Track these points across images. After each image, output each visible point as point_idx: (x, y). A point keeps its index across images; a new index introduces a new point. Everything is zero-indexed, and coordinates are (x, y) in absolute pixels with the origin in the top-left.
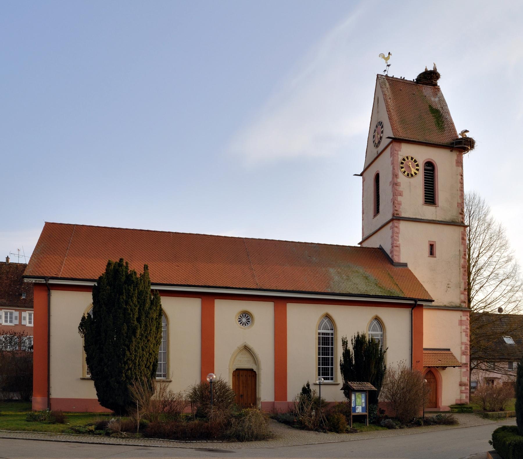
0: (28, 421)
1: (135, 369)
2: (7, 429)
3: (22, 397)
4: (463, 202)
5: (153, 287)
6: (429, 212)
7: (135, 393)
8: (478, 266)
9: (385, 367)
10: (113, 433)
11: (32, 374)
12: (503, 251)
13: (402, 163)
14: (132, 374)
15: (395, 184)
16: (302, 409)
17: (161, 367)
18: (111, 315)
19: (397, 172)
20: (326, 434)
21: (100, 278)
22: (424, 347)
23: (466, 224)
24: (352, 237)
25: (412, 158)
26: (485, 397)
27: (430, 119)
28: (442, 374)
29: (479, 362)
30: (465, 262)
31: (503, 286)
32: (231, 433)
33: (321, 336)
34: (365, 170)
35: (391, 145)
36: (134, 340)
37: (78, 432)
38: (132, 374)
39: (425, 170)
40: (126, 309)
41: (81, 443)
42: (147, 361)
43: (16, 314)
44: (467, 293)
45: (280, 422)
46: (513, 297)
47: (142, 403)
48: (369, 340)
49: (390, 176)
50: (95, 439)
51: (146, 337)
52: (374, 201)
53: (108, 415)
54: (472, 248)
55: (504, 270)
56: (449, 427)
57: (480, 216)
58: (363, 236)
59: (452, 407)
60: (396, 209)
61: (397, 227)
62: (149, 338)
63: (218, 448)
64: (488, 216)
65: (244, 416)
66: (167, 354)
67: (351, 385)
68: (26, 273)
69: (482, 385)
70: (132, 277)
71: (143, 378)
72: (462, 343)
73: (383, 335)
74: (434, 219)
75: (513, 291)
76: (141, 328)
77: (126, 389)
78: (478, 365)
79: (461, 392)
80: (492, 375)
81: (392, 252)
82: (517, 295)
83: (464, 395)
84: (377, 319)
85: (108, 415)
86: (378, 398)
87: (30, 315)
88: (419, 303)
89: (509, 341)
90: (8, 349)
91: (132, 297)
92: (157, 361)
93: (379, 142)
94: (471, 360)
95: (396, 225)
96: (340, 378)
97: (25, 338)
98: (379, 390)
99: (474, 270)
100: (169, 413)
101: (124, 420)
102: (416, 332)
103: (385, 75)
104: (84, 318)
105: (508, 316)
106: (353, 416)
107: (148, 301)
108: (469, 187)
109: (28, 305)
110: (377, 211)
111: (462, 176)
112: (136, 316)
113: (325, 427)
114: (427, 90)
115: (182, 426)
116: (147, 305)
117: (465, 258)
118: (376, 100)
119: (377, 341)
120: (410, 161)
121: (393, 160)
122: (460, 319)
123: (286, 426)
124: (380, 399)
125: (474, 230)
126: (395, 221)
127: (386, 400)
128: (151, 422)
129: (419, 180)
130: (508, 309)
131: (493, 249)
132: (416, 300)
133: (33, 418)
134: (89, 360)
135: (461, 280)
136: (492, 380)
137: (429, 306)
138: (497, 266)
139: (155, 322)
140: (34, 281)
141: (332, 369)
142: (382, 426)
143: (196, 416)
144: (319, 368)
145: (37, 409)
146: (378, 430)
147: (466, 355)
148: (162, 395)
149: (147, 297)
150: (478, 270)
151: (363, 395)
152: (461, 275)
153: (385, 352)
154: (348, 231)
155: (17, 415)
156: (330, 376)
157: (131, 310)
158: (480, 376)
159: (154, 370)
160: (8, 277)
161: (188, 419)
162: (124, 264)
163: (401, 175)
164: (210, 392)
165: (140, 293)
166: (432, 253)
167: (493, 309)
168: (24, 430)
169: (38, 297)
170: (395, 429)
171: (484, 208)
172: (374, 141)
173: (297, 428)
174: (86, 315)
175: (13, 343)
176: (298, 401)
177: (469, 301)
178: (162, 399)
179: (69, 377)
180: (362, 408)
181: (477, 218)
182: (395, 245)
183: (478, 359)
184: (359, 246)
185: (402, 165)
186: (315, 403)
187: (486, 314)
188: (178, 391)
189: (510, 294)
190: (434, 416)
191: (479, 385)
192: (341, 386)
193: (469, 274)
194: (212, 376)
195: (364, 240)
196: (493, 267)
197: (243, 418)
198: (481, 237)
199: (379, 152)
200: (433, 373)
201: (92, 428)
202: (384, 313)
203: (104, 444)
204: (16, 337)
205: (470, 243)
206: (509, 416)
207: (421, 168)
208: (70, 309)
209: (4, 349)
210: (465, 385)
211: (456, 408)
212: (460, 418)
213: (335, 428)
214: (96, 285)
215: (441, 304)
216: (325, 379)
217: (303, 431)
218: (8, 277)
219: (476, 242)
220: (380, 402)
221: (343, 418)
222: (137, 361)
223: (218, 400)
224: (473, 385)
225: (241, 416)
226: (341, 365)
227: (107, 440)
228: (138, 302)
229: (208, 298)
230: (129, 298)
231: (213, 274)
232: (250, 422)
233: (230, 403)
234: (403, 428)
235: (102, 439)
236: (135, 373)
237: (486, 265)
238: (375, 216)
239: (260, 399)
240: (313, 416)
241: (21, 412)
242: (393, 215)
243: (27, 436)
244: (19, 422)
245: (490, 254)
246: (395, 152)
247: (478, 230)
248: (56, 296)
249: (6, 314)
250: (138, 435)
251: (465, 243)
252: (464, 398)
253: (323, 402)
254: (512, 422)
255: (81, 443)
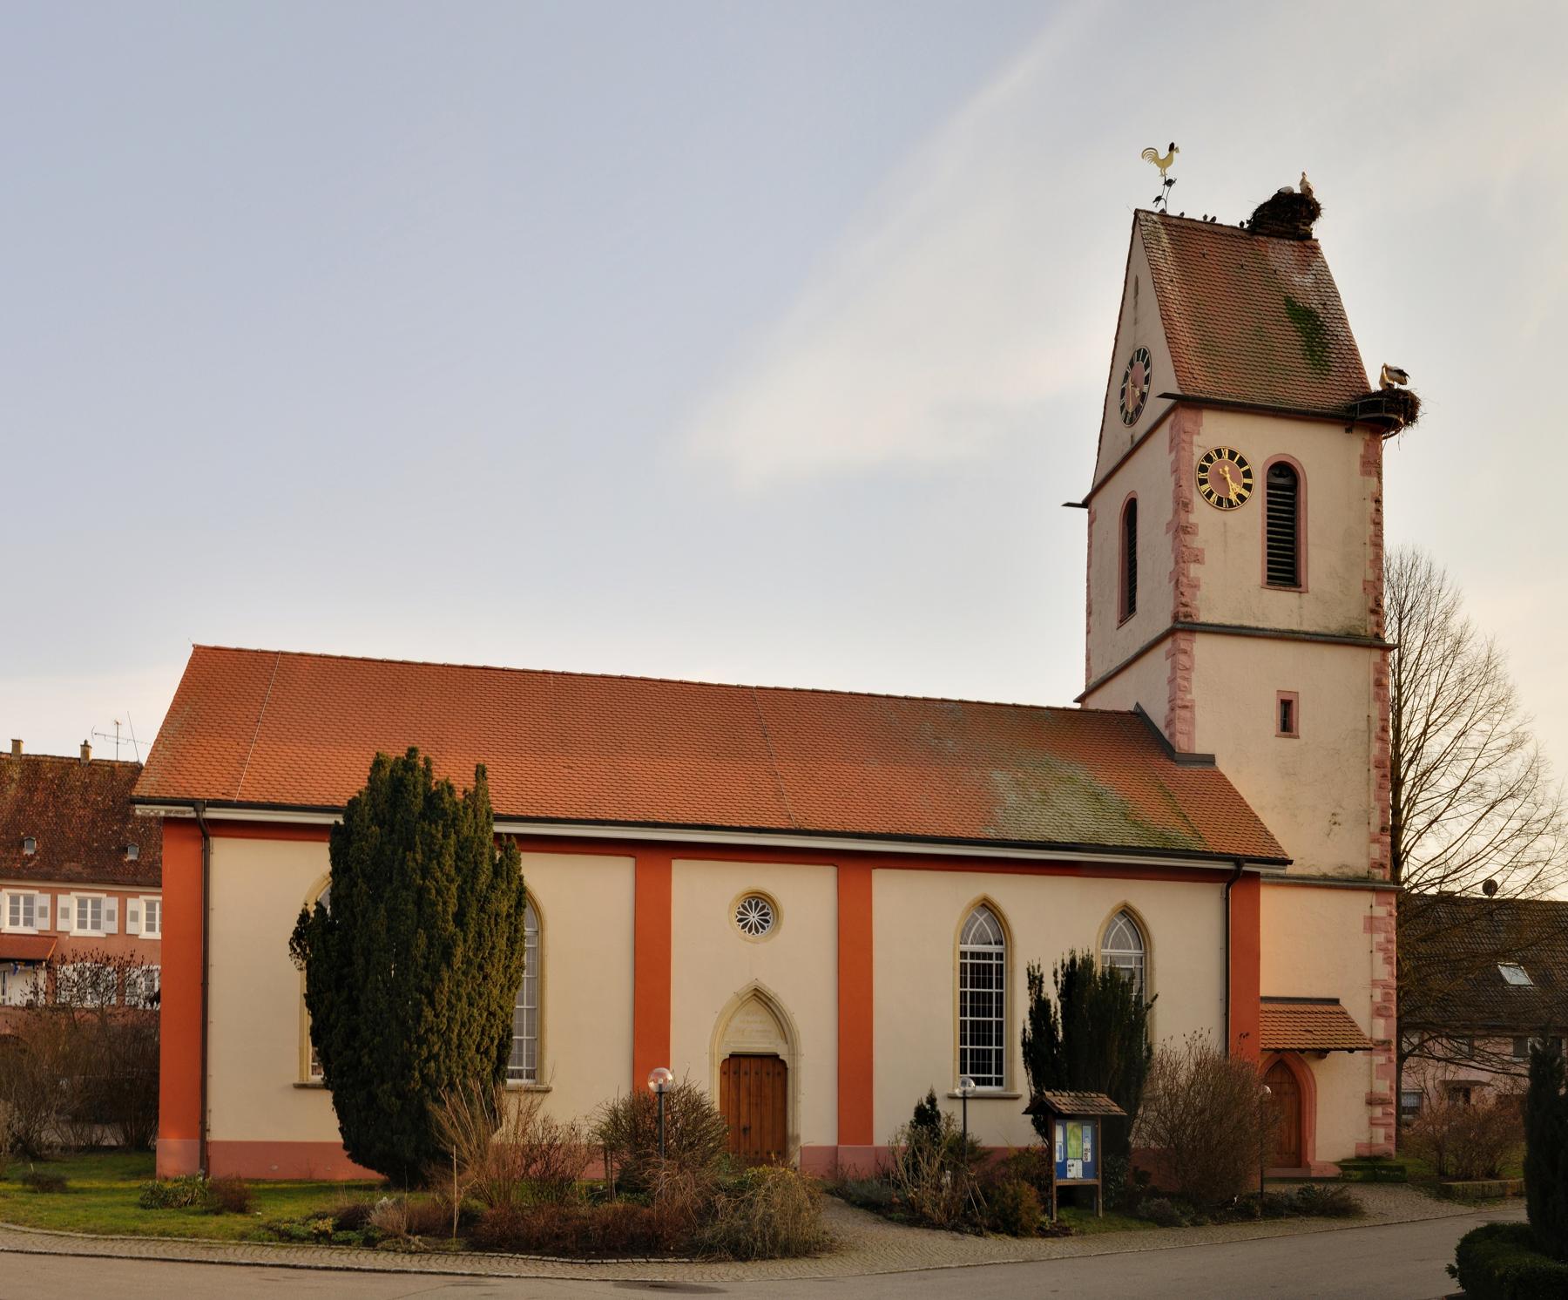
0: (144, 1207)
1: (447, 1056)
2: (85, 1231)
3: (127, 1138)
4: (1380, 579)
5: (499, 828)
6: (1281, 609)
7: (447, 1126)
8: (1424, 761)
9: (1150, 1049)
10: (384, 1238)
11: (157, 1075)
12: (1498, 717)
13: (1203, 469)
14: (438, 1071)
15: (1181, 530)
16: (915, 1168)
17: (521, 1049)
18: (382, 906)
19: (1187, 493)
20: (981, 1241)
21: (353, 803)
22: (1263, 993)
23: (1389, 641)
24: (1057, 681)
25: (1232, 455)
26: (1443, 1137)
27: (1288, 339)
28: (1317, 1077)
29: (1426, 1036)
30: (1384, 750)
31: (1496, 820)
32: (714, 1237)
33: (969, 961)
34: (1096, 490)
35: (1172, 417)
36: (446, 975)
37: (286, 1237)
38: (438, 1071)
39: (1270, 486)
40: (422, 891)
41: (295, 1267)
42: (483, 1033)
43: (110, 903)
44: (1389, 839)
45: (853, 1204)
46: (1528, 850)
47: (466, 1154)
48: (1103, 973)
49: (1169, 505)
50: (335, 1255)
51: (481, 968)
52: (1121, 578)
53: (369, 1188)
54: (1406, 710)
55: (1501, 772)
56: (1337, 1224)
57: (1431, 617)
58: (1088, 678)
59: (1345, 1165)
60: (1184, 600)
61: (1185, 652)
62: (488, 968)
63: (678, 1279)
64: (1455, 617)
65: (751, 1187)
66: (537, 1014)
67: (1054, 1100)
68: (140, 790)
69: (1435, 1102)
70: (442, 799)
71: (470, 1082)
72: (1374, 983)
73: (1145, 959)
74: (1295, 628)
75: (1527, 834)
76: (465, 941)
77: (423, 1114)
78: (1421, 1045)
79: (1373, 1123)
80: (1464, 1075)
81: (1170, 723)
82: (1539, 844)
83: (1380, 1133)
84: (1127, 912)
85: (369, 1188)
86: (1131, 1139)
87: (150, 906)
88: (1248, 868)
89: (1515, 976)
90: (88, 1004)
91: (441, 854)
92: (510, 1035)
93: (1138, 410)
94: (1401, 1031)
95: (1183, 645)
96: (1021, 1080)
97: (137, 972)
98: (1133, 1115)
99: (1411, 774)
100: (542, 1179)
101: (417, 1201)
102: (1238, 951)
103: (1157, 211)
104: (304, 916)
105: (1513, 906)
106: (1060, 1188)
107: (486, 866)
108: (1400, 535)
109: (146, 877)
110: (1129, 606)
111: (1378, 501)
112: (452, 909)
113: (978, 1219)
114: (1281, 254)
115: (578, 1217)
116: (483, 878)
117: (1383, 740)
118: (1132, 286)
119: (1126, 977)
120: (1225, 463)
121: (1177, 459)
122: (1368, 913)
123: (871, 1217)
124: (1135, 1141)
125: (1412, 658)
126: (1180, 636)
127: (1153, 1144)
128: (491, 1206)
129: (1253, 517)
130: (1513, 885)
131: (1468, 712)
132: (1238, 860)
133: (159, 1200)
134: (317, 1035)
135: (1373, 803)
136: (1463, 1090)
137: (1278, 876)
138: (1481, 763)
139: (504, 925)
140: (162, 811)
141: (999, 1053)
142: (1141, 1219)
143: (619, 1187)
144: (963, 1052)
145: (170, 1174)
146: (1129, 1229)
147: (1387, 1017)
148: (524, 1131)
149: (482, 854)
150: (1424, 774)
151: (1088, 1130)
152: (1373, 787)
153: (1149, 1007)
154: (1046, 666)
155: (114, 1191)
156: (993, 1075)
157: (439, 892)
158: (1429, 1076)
159: (502, 1060)
160: (86, 802)
161: (596, 1195)
162: (421, 764)
163: (1198, 502)
164: (658, 1120)
165: (463, 845)
166: (1287, 725)
167: (1469, 884)
168: (135, 1232)
169: (175, 856)
170: (1180, 1226)
171: (1443, 593)
172: (1122, 407)
173: (901, 1222)
174: (312, 908)
175: (103, 985)
176: (903, 1144)
177: (1397, 860)
178: (523, 1141)
179: (262, 1083)
180: (1085, 1166)
181: (1423, 623)
182: (1179, 702)
183: (1425, 1030)
184: (1078, 706)
185: (1201, 475)
186: (951, 1150)
187: (1446, 898)
188: (569, 1120)
189: (1519, 842)
190: (1293, 1189)
191: (1426, 1102)
192: (1025, 1103)
193: (1398, 783)
194: (662, 1075)
195: (1091, 691)
196: (1468, 764)
197: (747, 1195)
198: (1434, 678)
199: (1137, 439)
200: (1289, 1071)
201: (327, 1225)
202: (1149, 899)
203: (359, 1270)
204: (110, 969)
205: (1400, 694)
206: (1515, 1195)
207: (1259, 481)
208: (266, 891)
209: (76, 1004)
210: (1384, 1102)
211: (1356, 1168)
212: (1371, 1198)
213: (1009, 1224)
214: (341, 822)
215: (1314, 872)
216: (978, 1082)
217: (917, 1231)
218: (86, 802)
219: (1419, 692)
220: (1136, 1150)
221: (1029, 1195)
222: (454, 1036)
223: (679, 1141)
224: (1407, 1102)
225: (741, 1187)
226: (1024, 1044)
227: (366, 1259)
228: (458, 870)
229: (653, 854)
230: (430, 860)
231: (664, 790)
232: (770, 1205)
233: (714, 1151)
234: (1201, 1224)
235: (352, 1257)
236: (448, 1069)
237: (1449, 758)
238: (1123, 621)
239: (797, 1138)
240: (945, 1188)
241: (123, 1180)
242: (1176, 618)
243: (143, 1249)
244: (121, 1210)
245: (1461, 726)
246: (1184, 436)
247: (1426, 657)
248: (228, 856)
249: (82, 903)
250: (454, 1243)
251: (1385, 695)
252: (1382, 1138)
253: (973, 1147)
254: (1516, 1213)
255: (295, 1267)
